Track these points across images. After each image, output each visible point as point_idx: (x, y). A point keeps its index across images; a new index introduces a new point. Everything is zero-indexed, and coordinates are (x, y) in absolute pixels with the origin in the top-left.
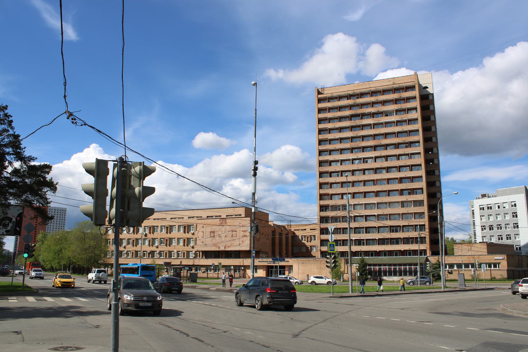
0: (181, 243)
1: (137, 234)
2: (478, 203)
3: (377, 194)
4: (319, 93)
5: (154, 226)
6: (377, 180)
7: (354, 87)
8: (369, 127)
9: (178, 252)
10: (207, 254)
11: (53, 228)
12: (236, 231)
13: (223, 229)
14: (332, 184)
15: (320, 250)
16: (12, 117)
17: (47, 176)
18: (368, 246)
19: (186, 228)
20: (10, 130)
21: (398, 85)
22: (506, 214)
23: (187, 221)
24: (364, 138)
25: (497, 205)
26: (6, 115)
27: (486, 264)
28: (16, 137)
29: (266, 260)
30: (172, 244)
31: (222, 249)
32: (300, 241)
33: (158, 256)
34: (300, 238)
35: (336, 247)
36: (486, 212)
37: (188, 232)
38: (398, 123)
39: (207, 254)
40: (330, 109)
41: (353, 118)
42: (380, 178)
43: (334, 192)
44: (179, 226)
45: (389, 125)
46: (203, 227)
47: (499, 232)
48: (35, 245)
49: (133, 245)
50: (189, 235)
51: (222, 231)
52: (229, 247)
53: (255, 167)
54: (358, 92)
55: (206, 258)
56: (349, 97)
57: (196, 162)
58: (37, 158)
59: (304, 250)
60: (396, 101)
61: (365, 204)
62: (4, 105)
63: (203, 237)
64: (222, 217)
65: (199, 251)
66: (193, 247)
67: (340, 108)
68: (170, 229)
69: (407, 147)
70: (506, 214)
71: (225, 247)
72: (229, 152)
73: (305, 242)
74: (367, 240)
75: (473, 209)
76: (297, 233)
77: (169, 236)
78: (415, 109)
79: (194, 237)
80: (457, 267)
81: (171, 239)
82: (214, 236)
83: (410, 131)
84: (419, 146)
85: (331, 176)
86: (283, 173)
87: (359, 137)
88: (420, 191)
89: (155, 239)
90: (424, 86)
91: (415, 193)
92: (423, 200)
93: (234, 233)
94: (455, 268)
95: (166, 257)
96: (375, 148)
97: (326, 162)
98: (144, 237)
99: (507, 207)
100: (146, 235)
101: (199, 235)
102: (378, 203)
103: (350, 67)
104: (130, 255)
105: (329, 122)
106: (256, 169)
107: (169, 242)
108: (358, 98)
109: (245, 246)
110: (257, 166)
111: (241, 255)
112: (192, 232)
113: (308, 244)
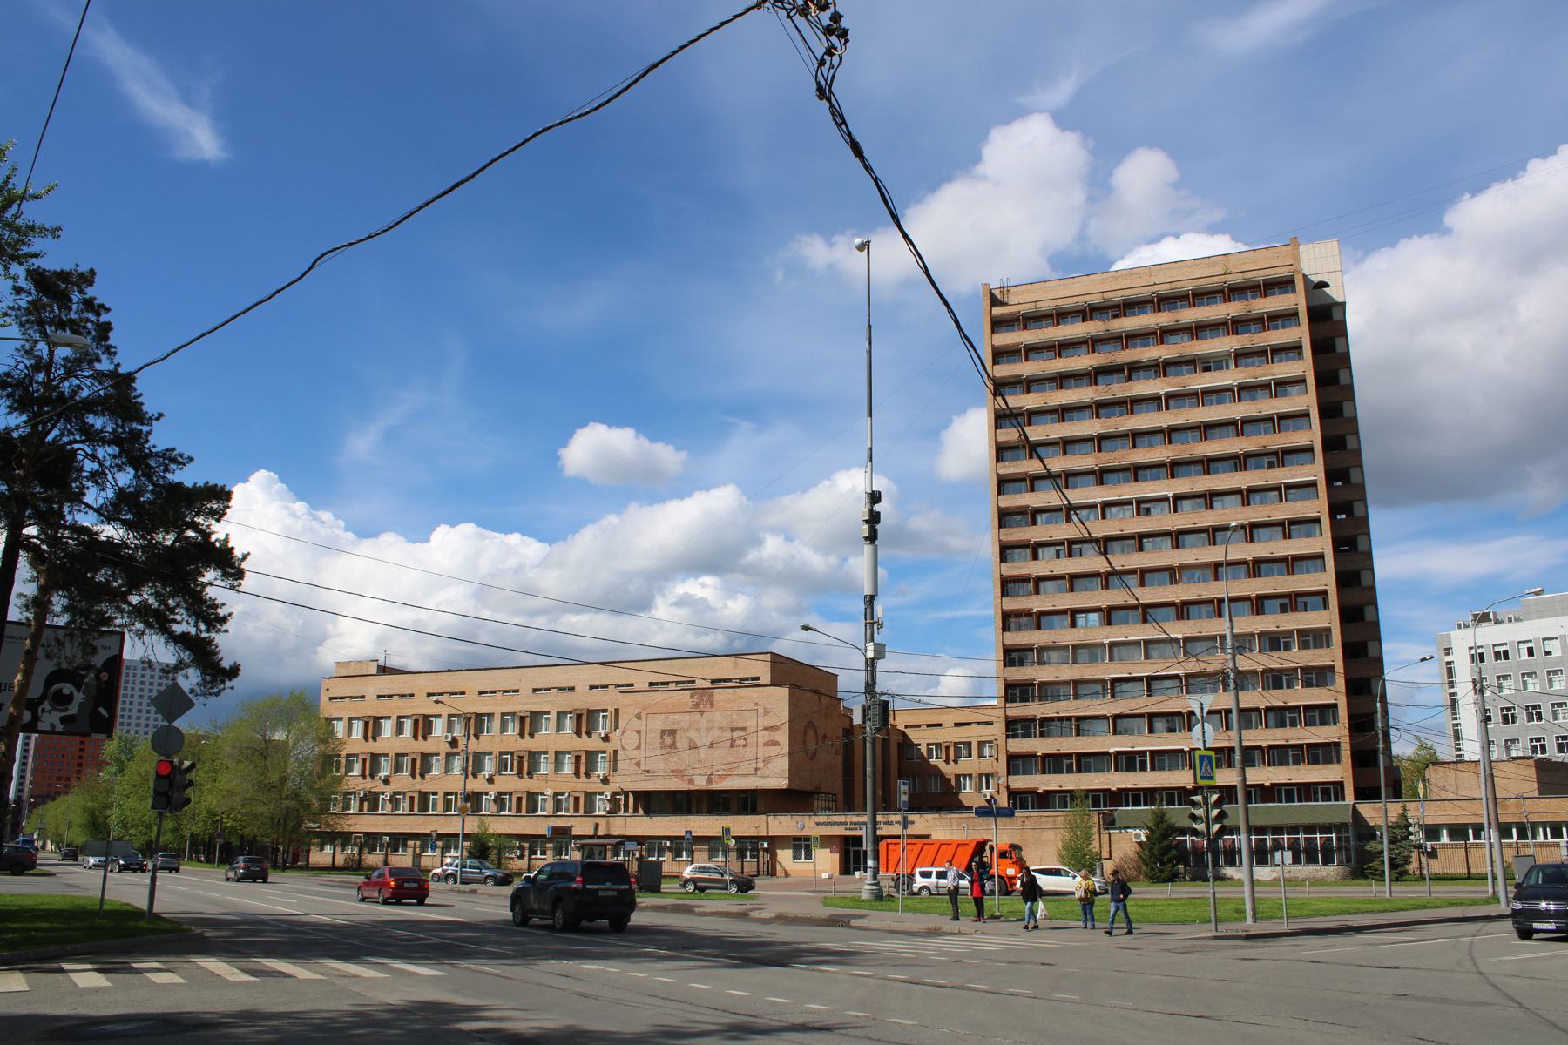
0: (568, 768)
1: (425, 738)
2: (1462, 642)
3: (1182, 610)
4: (994, 302)
5: (478, 716)
6: (1182, 567)
7: (1103, 281)
8: (1154, 405)
9: (556, 794)
10: (650, 802)
11: (138, 725)
12: (743, 729)
13: (703, 722)
14: (1039, 580)
15: (1008, 787)
16: (108, 310)
17: (215, 526)
18: (1156, 774)
19: (528, 721)
20: (104, 357)
21: (1240, 276)
22: (1556, 672)
23: (584, 700)
24: (1103, 443)
25: (1524, 647)
26: (89, 304)
27: (1544, 825)
28: (123, 382)
29: (842, 818)
30: (429, 771)
31: (700, 783)
32: (924, 761)
33: (493, 807)
34: (924, 750)
35: (1217, 771)
36: (1491, 667)
37: (589, 734)
38: (1245, 391)
39: (650, 802)
40: (1030, 351)
41: (1100, 379)
42: (1191, 561)
43: (1047, 607)
44: (559, 713)
45: (1214, 397)
46: (639, 717)
47: (1535, 730)
48: (193, 766)
49: (413, 775)
50: (593, 743)
51: (698, 730)
52: (723, 777)
53: (871, 511)
54: (1116, 297)
55: (648, 812)
56: (1087, 313)
57: (576, 527)
58: (191, 459)
59: (935, 788)
60: (1235, 326)
61: (1147, 642)
62: (84, 268)
63: (638, 747)
64: (636, 687)
65: (626, 794)
66: (605, 781)
67: (1060, 348)
68: (530, 723)
69: (1271, 465)
70: (1556, 672)
71: (710, 781)
72: (682, 488)
73: (940, 764)
74: (1152, 752)
75: (1448, 659)
76: (913, 735)
77: (528, 744)
78: (1296, 348)
79: (609, 747)
80: (1452, 835)
81: (534, 756)
82: (673, 745)
83: (1283, 417)
84: (1313, 461)
85: (1035, 557)
86: (845, 560)
87: (1123, 436)
88: (1319, 599)
89: (485, 753)
90: (1315, 279)
91: (1300, 605)
92: (1328, 630)
93: (738, 734)
94: (1445, 839)
95: (519, 810)
96: (1173, 468)
97: (1021, 511)
98: (448, 749)
99: (1557, 653)
100: (454, 743)
101: (625, 740)
102: (1112, 645)
103: (1062, 234)
104: (404, 804)
105: (1028, 391)
106: (874, 518)
107: (528, 763)
108: (1115, 316)
109: (776, 776)
110: (877, 507)
111: (760, 804)
112: (602, 732)
113: (949, 770)
